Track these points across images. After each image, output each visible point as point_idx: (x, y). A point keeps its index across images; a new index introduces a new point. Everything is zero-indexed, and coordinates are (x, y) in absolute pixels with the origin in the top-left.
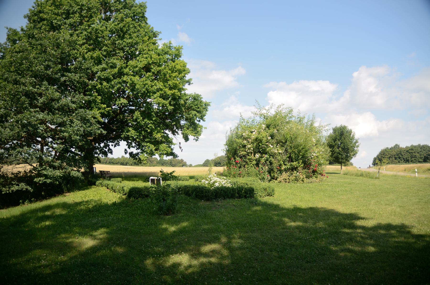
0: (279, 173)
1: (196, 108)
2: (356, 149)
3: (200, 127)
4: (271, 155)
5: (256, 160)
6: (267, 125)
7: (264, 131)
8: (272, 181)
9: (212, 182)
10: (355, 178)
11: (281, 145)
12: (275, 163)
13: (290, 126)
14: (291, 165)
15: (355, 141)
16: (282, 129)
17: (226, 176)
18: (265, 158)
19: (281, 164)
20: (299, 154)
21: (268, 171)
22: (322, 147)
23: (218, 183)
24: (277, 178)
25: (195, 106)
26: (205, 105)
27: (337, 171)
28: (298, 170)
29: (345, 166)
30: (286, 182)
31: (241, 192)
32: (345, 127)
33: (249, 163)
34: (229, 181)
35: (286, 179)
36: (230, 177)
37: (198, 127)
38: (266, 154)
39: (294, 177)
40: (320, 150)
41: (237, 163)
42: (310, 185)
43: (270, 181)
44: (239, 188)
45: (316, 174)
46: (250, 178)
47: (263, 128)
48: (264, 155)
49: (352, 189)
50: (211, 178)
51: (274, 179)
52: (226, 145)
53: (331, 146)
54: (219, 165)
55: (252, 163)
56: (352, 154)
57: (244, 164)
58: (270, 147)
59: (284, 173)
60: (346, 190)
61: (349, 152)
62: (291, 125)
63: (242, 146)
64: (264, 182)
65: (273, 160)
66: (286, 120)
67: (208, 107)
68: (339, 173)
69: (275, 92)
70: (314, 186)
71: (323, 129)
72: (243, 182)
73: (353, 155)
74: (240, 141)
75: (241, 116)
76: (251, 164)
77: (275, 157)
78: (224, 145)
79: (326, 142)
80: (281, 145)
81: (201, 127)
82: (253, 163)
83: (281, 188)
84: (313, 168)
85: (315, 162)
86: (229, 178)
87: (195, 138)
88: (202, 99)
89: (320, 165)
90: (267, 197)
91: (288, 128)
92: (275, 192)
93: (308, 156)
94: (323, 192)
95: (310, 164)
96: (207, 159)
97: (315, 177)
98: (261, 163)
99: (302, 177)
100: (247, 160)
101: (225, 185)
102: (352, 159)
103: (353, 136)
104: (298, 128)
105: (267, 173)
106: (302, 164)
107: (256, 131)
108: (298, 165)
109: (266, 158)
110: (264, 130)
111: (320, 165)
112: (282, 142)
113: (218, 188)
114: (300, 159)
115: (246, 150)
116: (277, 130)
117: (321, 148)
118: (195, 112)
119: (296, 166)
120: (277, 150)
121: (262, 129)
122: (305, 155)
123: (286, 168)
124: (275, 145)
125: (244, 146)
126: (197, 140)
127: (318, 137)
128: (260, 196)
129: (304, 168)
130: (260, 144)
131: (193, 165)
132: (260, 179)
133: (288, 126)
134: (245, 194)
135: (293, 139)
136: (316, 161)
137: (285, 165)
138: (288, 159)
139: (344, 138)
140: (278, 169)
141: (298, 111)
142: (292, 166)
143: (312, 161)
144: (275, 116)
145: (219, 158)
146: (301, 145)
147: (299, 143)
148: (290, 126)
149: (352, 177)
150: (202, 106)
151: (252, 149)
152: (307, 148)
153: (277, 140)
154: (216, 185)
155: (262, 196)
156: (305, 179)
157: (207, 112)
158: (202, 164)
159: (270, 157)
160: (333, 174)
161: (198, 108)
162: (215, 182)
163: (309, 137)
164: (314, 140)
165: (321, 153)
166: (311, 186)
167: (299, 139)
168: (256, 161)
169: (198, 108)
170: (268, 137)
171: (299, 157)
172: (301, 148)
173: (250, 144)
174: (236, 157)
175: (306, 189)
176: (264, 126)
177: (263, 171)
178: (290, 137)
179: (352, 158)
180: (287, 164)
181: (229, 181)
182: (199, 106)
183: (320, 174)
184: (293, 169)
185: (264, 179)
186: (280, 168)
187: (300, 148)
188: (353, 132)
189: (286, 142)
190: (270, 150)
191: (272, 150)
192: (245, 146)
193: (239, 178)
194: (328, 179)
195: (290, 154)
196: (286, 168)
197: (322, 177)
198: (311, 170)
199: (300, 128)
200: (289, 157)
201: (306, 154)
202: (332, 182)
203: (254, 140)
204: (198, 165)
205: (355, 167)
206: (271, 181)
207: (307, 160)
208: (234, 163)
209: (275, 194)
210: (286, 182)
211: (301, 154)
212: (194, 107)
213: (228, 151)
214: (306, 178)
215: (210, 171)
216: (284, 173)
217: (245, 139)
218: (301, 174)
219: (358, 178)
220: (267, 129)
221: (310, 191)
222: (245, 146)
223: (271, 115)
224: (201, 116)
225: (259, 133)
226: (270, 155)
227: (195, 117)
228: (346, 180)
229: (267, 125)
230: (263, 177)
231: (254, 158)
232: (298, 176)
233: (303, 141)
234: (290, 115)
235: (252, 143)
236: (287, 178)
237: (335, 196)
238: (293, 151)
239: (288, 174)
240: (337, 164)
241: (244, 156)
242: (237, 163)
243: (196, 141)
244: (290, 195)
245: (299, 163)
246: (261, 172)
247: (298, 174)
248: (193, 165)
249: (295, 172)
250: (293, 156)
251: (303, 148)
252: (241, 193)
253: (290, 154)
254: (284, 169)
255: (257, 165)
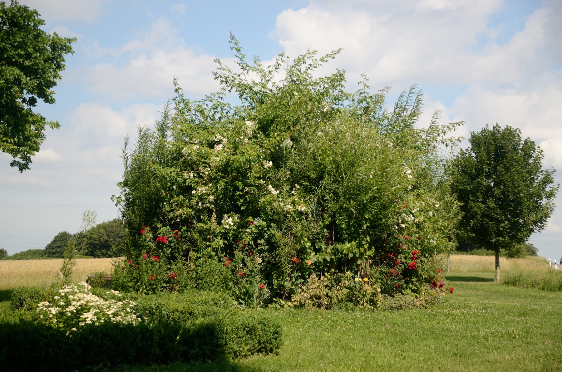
0: (297, 278)
1: (20, 56)
2: (544, 201)
3: (34, 123)
4: (272, 221)
5: (224, 236)
6: (260, 122)
7: (251, 142)
8: (274, 305)
9: (71, 308)
10: (542, 297)
11: (305, 187)
12: (286, 244)
13: (333, 127)
14: (336, 252)
15: (541, 177)
16: (310, 137)
17: (123, 288)
18: (252, 229)
19: (305, 248)
20: (363, 216)
21: (261, 271)
22: (436, 195)
23: (93, 311)
24: (291, 292)
25: (17, 48)
26: (54, 47)
27: (485, 271)
28: (357, 266)
29: (511, 255)
30: (319, 306)
31: (173, 340)
32: (510, 133)
33: (201, 244)
34: (133, 303)
35: (319, 298)
36: (138, 290)
37: (27, 122)
38: (256, 215)
39: (346, 291)
40: (427, 204)
41: (160, 245)
42: (396, 316)
43: (267, 302)
44: (166, 326)
45: (414, 279)
46: (204, 295)
47: (250, 132)
48: (251, 219)
49: (528, 332)
50: (71, 297)
51: (280, 296)
52: (126, 184)
53: (462, 195)
54: (103, 251)
55: (213, 244)
56: (533, 217)
57: (184, 247)
58: (270, 192)
59: (314, 276)
60: (510, 334)
61: (521, 211)
62: (336, 123)
63: (179, 187)
64: (249, 305)
65: (278, 234)
66: (323, 108)
67: (65, 56)
68: (491, 280)
69: (304, 11)
70: (407, 319)
71: (439, 138)
72: (180, 306)
73: (535, 222)
74: (171, 171)
75: (176, 91)
76: (208, 246)
77: (284, 227)
78: (120, 183)
79: (449, 180)
80: (305, 187)
81: (40, 121)
82: (213, 244)
83: (303, 325)
84: (404, 260)
85: (411, 242)
86: (133, 294)
87: (18, 159)
88: (41, 27)
89: (428, 251)
90: (256, 357)
91: (327, 134)
92: (283, 338)
93: (390, 222)
94: (436, 338)
95: (396, 250)
96: (62, 230)
97: (413, 291)
98: (241, 245)
99: (370, 291)
100: (196, 236)
101: (119, 318)
102: (533, 236)
103: (537, 160)
104: (358, 135)
105: (258, 278)
106: (370, 248)
107: (225, 141)
108: (357, 251)
109: (257, 227)
110: (250, 139)
111: (428, 251)
112: (308, 178)
113: (91, 327)
114: (364, 233)
115: (193, 202)
116: (292, 139)
117: (431, 199)
118: (17, 71)
119: (351, 255)
120: (294, 203)
121: (246, 135)
122: (381, 219)
123: (321, 260)
124: (286, 188)
125: (186, 190)
126: (23, 168)
127: (423, 164)
128: (235, 353)
129: (377, 261)
130: (240, 184)
131: (10, 253)
132: (237, 298)
133: (329, 128)
134: (183, 348)
135: (342, 170)
136: (413, 238)
137: (317, 251)
138: (326, 232)
139: (507, 169)
140: (294, 263)
141: (362, 79)
142: (339, 256)
143: (402, 238)
144: (287, 93)
145: (104, 226)
146: (367, 189)
147: (362, 181)
148: (333, 127)
149: (532, 292)
150: (41, 51)
151: (212, 198)
152: (387, 196)
153: (292, 170)
154: (85, 320)
155: (240, 352)
156: (380, 295)
157: (60, 73)
158: (43, 247)
159: (269, 226)
160: (471, 283)
161: (28, 56)
162: (82, 309)
163: (392, 162)
164: (409, 171)
165: (431, 214)
166: (399, 320)
167: (362, 168)
168: (225, 238)
169: (28, 56)
170: (264, 163)
171: (360, 226)
172: (367, 197)
173: (205, 184)
174: (159, 225)
175: (383, 329)
176: (251, 126)
177: (245, 270)
178: (335, 161)
179: (532, 230)
180: (323, 247)
181: (133, 303)
182: (30, 50)
183: (428, 281)
184: (344, 264)
185: (251, 296)
186: (303, 259)
187: (366, 198)
188: (537, 150)
189: (321, 178)
190: (270, 204)
191: (275, 204)
192: (190, 188)
193: (165, 293)
194: (454, 299)
195: (333, 216)
196: (321, 260)
197: (432, 292)
198: (399, 270)
199: (364, 134)
200: (328, 227)
201: (385, 217)
202: (466, 306)
203: (218, 170)
204: (29, 251)
205: (545, 261)
206: (271, 302)
207: (385, 236)
208: (152, 244)
209: (282, 344)
210: (319, 306)
211: (367, 216)
212: (12, 53)
213: (130, 204)
214: (382, 292)
215: (67, 273)
216: (314, 276)
217: (190, 165)
218: (366, 279)
219: (552, 295)
220: (261, 135)
221: (396, 335)
222: (190, 188)
223: (274, 89)
224: (40, 86)
225: (236, 148)
226: (269, 221)
227: (16, 88)
228: (516, 303)
229: (260, 122)
230: (247, 291)
231: (219, 229)
232: (358, 286)
233: (374, 176)
234: (336, 92)
235: (211, 179)
236: (321, 294)
237: (472, 353)
238: (341, 208)
239: (326, 279)
240: (484, 250)
241: (186, 222)
242: (160, 245)
243: (21, 170)
244: (332, 348)
245: (360, 245)
246: (238, 275)
247: (357, 279)
248: (10, 253)
249: (349, 273)
250: (342, 222)
251: (373, 199)
252: (169, 344)
253: (333, 216)
254: (315, 264)
255: (228, 250)
